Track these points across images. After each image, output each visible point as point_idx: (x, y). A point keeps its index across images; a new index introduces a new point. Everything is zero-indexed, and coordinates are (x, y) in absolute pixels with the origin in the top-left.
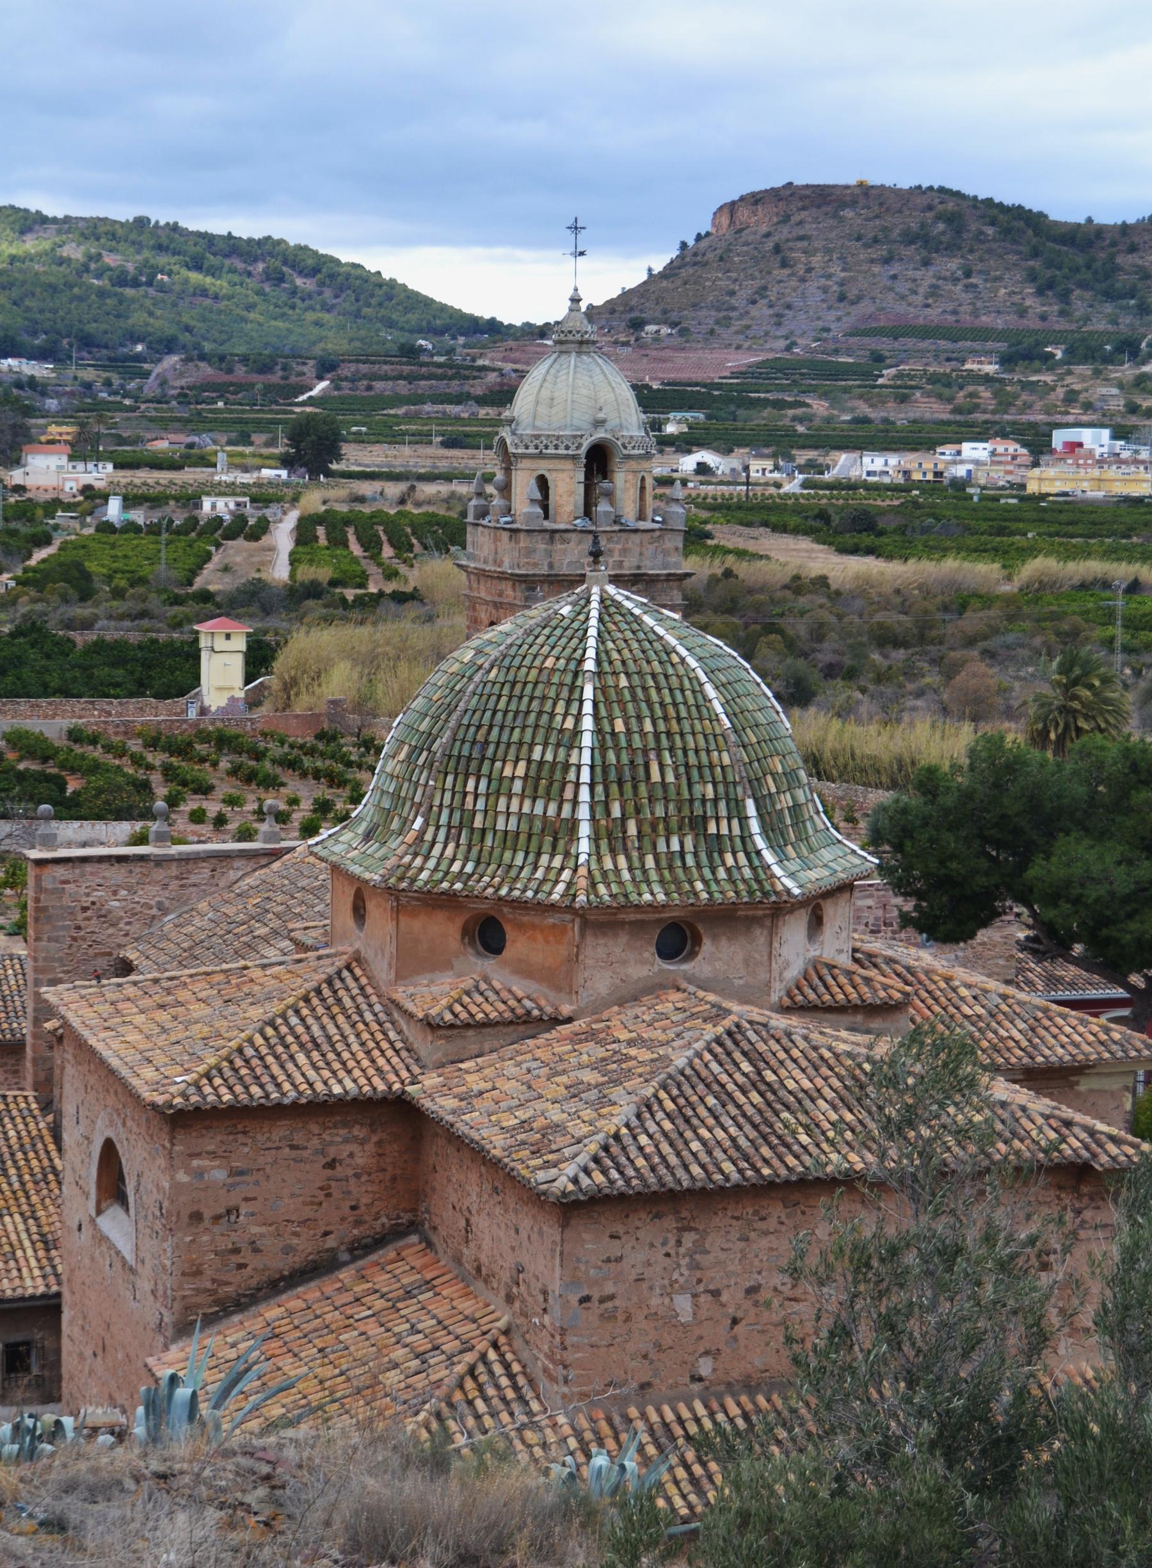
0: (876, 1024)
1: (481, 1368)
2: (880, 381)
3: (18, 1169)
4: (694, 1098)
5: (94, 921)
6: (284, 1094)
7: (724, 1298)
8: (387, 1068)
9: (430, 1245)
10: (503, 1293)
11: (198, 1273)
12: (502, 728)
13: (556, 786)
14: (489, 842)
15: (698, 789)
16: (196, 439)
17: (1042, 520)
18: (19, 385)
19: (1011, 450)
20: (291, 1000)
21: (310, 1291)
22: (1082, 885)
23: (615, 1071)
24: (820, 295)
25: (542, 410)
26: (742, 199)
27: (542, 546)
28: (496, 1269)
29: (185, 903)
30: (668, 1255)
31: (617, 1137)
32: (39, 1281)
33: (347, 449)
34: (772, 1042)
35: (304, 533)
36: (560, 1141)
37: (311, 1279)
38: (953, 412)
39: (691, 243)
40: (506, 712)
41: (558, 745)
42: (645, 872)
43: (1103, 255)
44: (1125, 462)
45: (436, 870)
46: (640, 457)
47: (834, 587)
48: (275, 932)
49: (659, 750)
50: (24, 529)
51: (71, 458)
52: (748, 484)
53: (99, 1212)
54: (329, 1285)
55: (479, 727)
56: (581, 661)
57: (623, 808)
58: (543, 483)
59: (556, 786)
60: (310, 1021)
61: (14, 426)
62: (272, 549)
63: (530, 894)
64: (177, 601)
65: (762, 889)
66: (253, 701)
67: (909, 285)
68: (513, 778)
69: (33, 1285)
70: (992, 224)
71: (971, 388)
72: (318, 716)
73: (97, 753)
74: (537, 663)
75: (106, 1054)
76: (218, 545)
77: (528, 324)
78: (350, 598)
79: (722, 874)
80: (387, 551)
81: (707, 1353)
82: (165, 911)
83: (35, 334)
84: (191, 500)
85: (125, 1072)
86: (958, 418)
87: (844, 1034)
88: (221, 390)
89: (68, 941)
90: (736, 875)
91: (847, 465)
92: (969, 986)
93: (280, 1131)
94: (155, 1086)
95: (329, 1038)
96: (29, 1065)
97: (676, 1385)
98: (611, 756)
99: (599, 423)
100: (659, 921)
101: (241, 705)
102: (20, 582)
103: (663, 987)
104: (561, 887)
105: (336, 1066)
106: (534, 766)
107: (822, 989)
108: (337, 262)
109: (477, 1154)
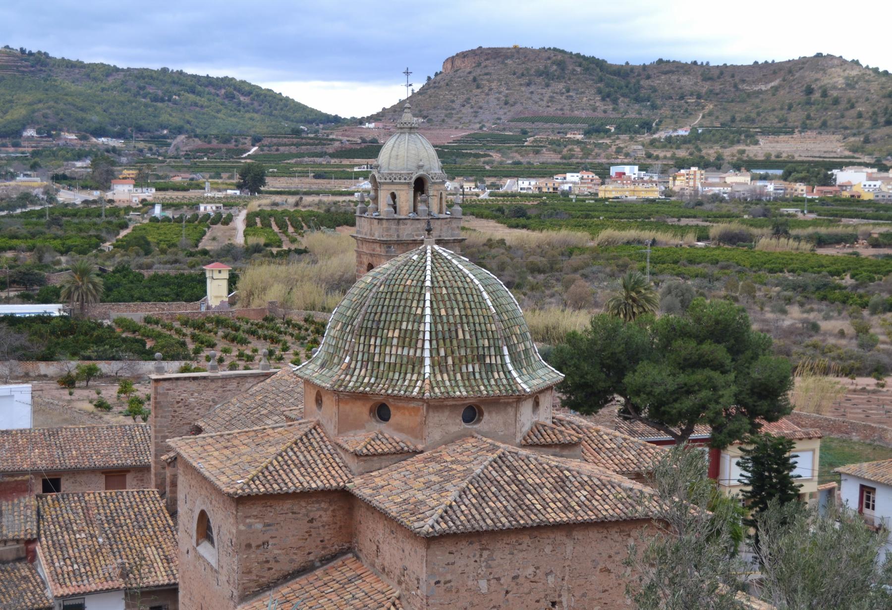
0: (565, 452)
2: (526, 144)
4: (486, 488)
6: (289, 488)
7: (502, 582)
8: (336, 475)
9: (358, 558)
11: (250, 572)
12: (387, 314)
13: (414, 341)
14: (382, 368)
15: (481, 342)
16: (194, 176)
17: (607, 211)
18: (108, 151)
19: (590, 177)
20: (289, 444)
21: (302, 580)
22: (652, 386)
23: (447, 476)
24: (496, 102)
25: (392, 161)
26: (457, 55)
27: (394, 227)
28: (392, 568)
29: (225, 399)
30: (476, 561)
31: (451, 506)
32: (166, 577)
33: (268, 180)
34: (520, 461)
35: (250, 222)
36: (423, 509)
38: (561, 158)
39: (433, 77)
40: (388, 306)
41: (414, 322)
42: (456, 381)
43: (633, 80)
44: (646, 182)
45: (356, 381)
46: (440, 183)
47: (508, 244)
48: (271, 412)
49: (462, 324)
51: (135, 186)
52: (463, 194)
54: (311, 577)
55: (376, 313)
56: (424, 282)
57: (445, 351)
58: (393, 196)
59: (414, 341)
60: (299, 453)
61: (107, 171)
62: (235, 229)
63: (402, 392)
64: (191, 255)
65: (512, 389)
66: (232, 303)
67: (539, 96)
68: (393, 338)
70: (580, 66)
71: (570, 147)
72: (263, 310)
73: (159, 328)
74: (403, 283)
76: (209, 228)
77: (353, 118)
78: (275, 252)
79: (493, 382)
80: (291, 230)
82: (216, 403)
83: (114, 125)
84: (195, 206)
85: (212, 478)
86: (564, 161)
87: (551, 457)
88: (206, 152)
89: (171, 418)
90: (499, 383)
91: (510, 185)
92: (608, 434)
93: (288, 505)
94: (228, 485)
95: (308, 461)
96: (153, 476)
98: (440, 327)
99: (420, 167)
100: (463, 405)
101: (227, 305)
102: (115, 246)
104: (417, 389)
105: (312, 474)
106: (403, 332)
107: (540, 436)
108: (260, 88)
109: (384, 515)
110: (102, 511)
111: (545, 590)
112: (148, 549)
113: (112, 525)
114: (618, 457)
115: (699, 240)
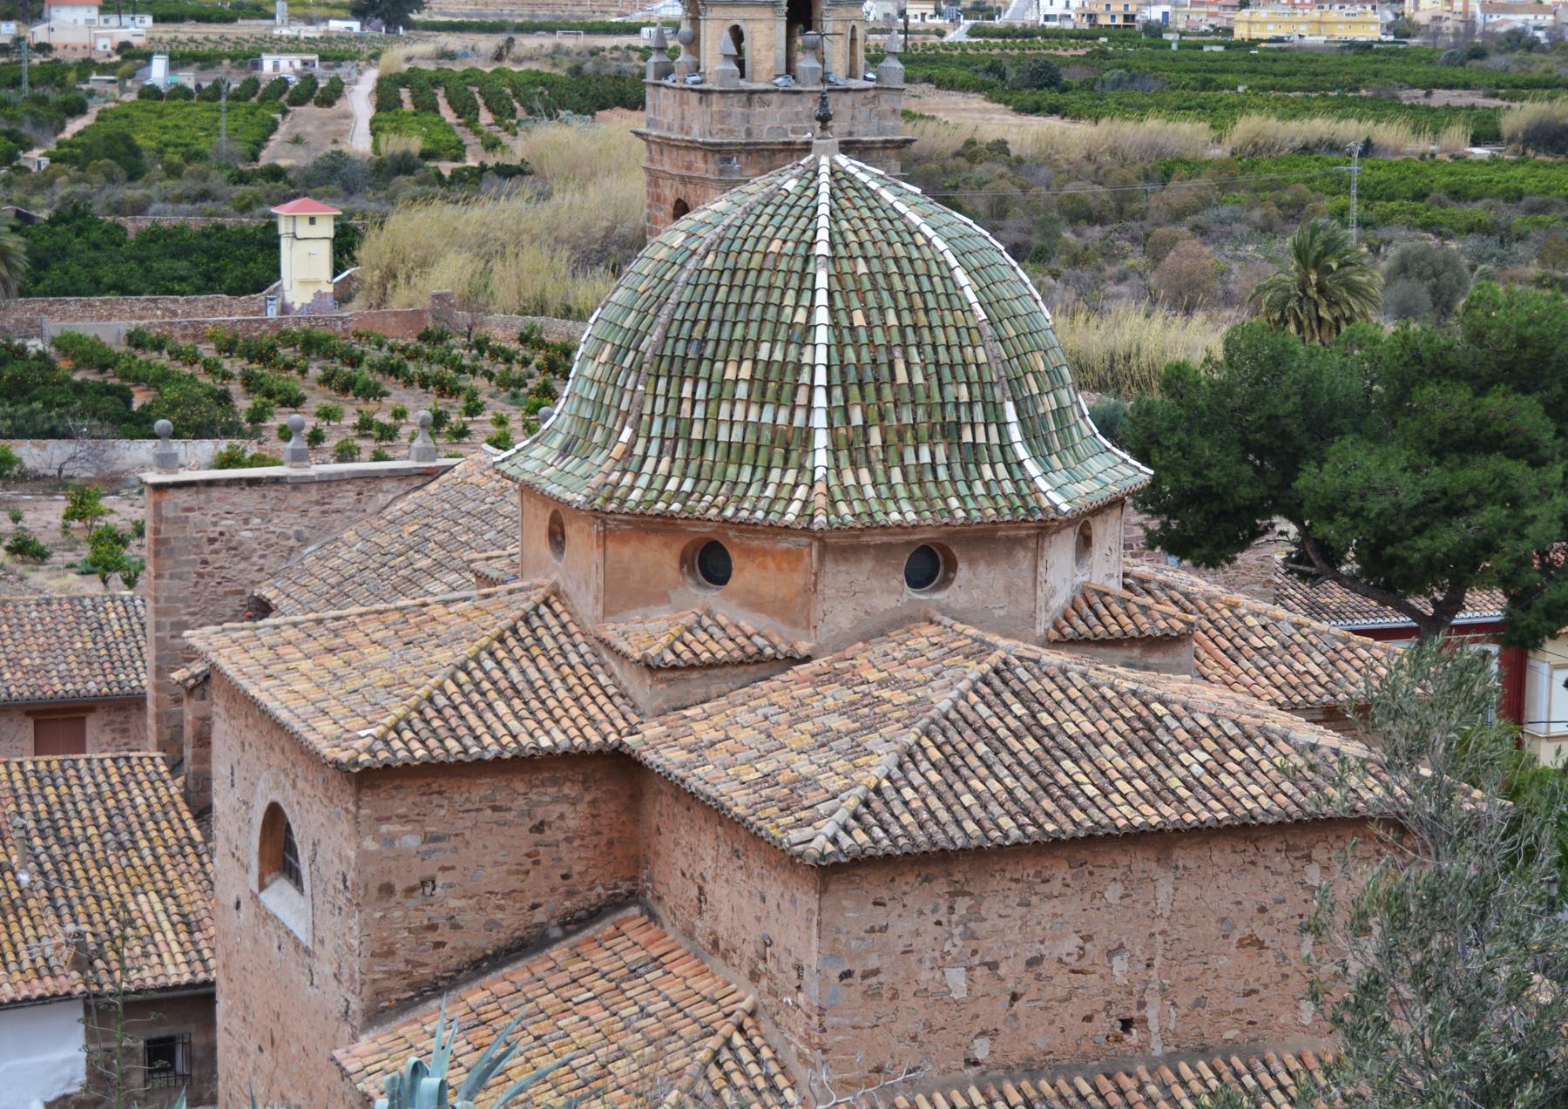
0: (1155, 658)
1: (725, 1055)
3: (150, 840)
4: (962, 746)
5: (223, 554)
6: (484, 748)
7: (1002, 971)
8: (600, 716)
9: (653, 917)
10: (746, 970)
11: (390, 953)
12: (722, 323)
13: (787, 388)
14: (709, 455)
15: (950, 391)
17: (1254, 71)
20: (484, 641)
21: (518, 972)
22: (1362, 497)
28: (736, 942)
29: (328, 532)
30: (939, 923)
31: (877, 790)
32: (184, 968)
34: (1046, 681)
35: (385, 98)
36: (812, 796)
37: (518, 959)
40: (726, 305)
41: (788, 342)
42: (891, 487)
45: (648, 488)
47: (1014, 152)
48: (439, 564)
49: (904, 346)
50: (54, 96)
52: (906, 32)
53: (262, 887)
55: (695, 322)
56: (811, 244)
58: (737, 35)
60: (507, 664)
62: (348, 116)
63: (760, 514)
64: (242, 179)
65: (1025, 506)
66: (343, 296)
68: (737, 381)
69: (177, 972)
72: (419, 313)
73: (163, 360)
74: (761, 247)
75: (272, 705)
76: (285, 112)
78: (447, 173)
79: (979, 488)
80: (485, 117)
81: (983, 1033)
82: (303, 541)
84: (249, 59)
85: (297, 726)
87: (1121, 670)
89: (194, 578)
90: (995, 491)
92: (1257, 615)
93: (482, 789)
95: (531, 683)
96: (151, 721)
97: (949, 1070)
98: (850, 355)
100: (908, 543)
101: (330, 301)
102: (54, 159)
103: (912, 619)
104: (795, 507)
105: (542, 715)
106: (760, 366)
107: (1093, 620)
109: (715, 813)
110: (26, 807)
111: (1106, 992)
112: (141, 898)
113: (51, 841)
114: (1282, 668)
115: (1476, 142)
